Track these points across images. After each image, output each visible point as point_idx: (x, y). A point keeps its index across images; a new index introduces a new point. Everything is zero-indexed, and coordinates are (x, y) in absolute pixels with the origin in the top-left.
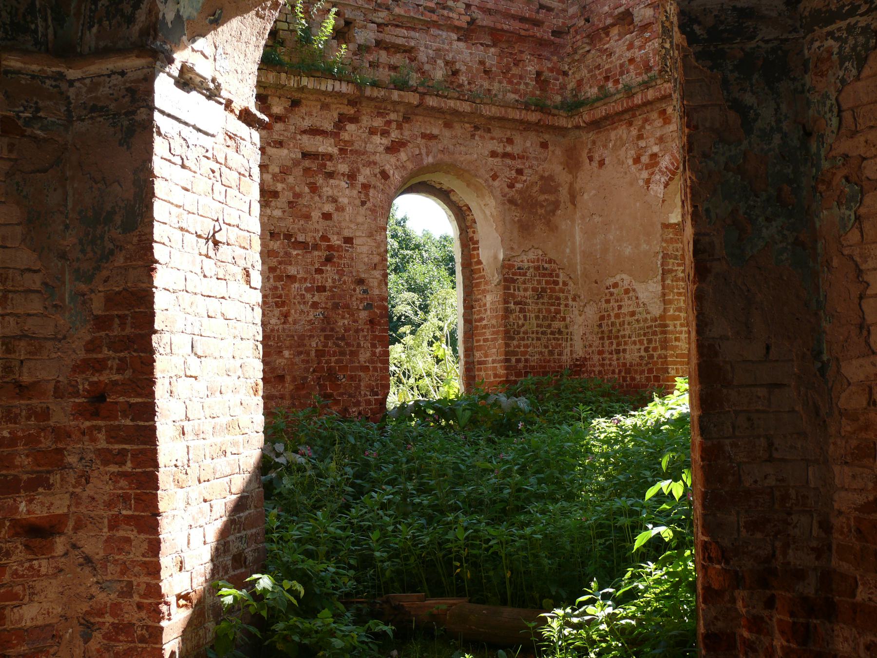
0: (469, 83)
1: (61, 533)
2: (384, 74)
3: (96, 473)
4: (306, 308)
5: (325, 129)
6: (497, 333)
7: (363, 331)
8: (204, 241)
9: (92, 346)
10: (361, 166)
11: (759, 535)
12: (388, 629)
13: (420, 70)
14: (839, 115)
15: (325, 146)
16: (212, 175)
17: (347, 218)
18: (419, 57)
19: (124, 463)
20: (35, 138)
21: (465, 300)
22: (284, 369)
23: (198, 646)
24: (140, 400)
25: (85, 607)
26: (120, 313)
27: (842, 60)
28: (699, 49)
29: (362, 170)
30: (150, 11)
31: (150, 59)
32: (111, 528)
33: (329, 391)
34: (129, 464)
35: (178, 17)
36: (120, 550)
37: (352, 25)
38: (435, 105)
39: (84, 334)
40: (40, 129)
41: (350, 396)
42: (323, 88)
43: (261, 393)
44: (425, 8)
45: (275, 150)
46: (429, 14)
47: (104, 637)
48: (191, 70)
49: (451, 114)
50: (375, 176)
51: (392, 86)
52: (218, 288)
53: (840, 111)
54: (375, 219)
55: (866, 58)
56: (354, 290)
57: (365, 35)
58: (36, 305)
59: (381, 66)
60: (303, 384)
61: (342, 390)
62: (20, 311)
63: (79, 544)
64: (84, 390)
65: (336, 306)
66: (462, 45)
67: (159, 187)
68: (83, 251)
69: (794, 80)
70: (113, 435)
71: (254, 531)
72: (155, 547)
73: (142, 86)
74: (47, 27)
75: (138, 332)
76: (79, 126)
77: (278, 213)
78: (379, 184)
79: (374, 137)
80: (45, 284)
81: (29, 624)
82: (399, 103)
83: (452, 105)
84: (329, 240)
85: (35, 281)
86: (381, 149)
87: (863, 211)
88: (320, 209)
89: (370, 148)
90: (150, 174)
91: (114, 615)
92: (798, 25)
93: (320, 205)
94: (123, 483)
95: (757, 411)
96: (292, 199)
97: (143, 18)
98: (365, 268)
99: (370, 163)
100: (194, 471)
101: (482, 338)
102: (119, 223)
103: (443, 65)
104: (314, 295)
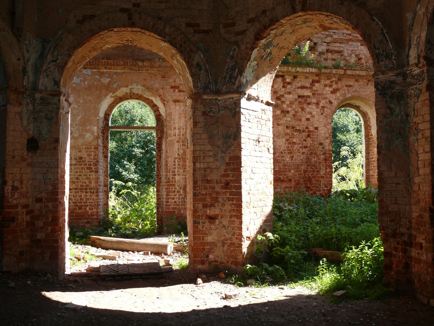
0: (366, 63)
1: (217, 219)
2: (330, 63)
3: (226, 204)
4: (300, 154)
5: (307, 86)
7: (322, 163)
8: (255, 141)
9: (226, 170)
10: (321, 99)
11: (392, 224)
12: (306, 253)
13: (345, 60)
14: (414, 111)
15: (307, 93)
16: (257, 122)
18: (344, 54)
19: (233, 201)
20: (211, 116)
21: (366, 150)
22: (291, 177)
23: (252, 251)
24: (238, 185)
25: (223, 238)
27: (415, 96)
28: (380, 92)
29: (321, 101)
30: (239, 82)
31: (239, 95)
32: (230, 218)
33: (308, 185)
34: (235, 201)
35: (247, 81)
36: (232, 224)
37: (317, 44)
38: (351, 73)
39: (224, 167)
40: (212, 113)
41: (317, 187)
42: (305, 71)
43: (273, 184)
44: (347, 34)
45: (288, 95)
46: (348, 36)
47: (228, 246)
48: (251, 95)
49: (358, 76)
50: (327, 103)
51: (333, 68)
52: (260, 154)
53: (414, 110)
54: (327, 120)
55: (419, 97)
56: (319, 147)
57: (322, 48)
58: (211, 160)
59: (329, 59)
60: (299, 183)
61: (313, 185)
62: (208, 161)
63: (222, 222)
64: (224, 182)
65: (311, 154)
67: (243, 129)
68: (223, 145)
69: (405, 100)
70: (231, 194)
71: (269, 224)
72: (241, 223)
73: (238, 102)
74: (213, 86)
75: (237, 167)
76: (222, 112)
77: (289, 119)
78: (328, 106)
80: (214, 154)
81: (209, 241)
82: (336, 74)
83: (358, 73)
84: (308, 128)
85: (211, 153)
87: (418, 137)
88: (305, 117)
89: (325, 92)
90: (240, 125)
91: (230, 240)
92: (406, 85)
93: (305, 115)
94: (233, 206)
95: (393, 190)
96: (294, 114)
97: (237, 83)
98: (323, 139)
99: (325, 98)
100: (252, 204)
101: (372, 166)
102: (232, 138)
103: (354, 56)
104: (303, 149)
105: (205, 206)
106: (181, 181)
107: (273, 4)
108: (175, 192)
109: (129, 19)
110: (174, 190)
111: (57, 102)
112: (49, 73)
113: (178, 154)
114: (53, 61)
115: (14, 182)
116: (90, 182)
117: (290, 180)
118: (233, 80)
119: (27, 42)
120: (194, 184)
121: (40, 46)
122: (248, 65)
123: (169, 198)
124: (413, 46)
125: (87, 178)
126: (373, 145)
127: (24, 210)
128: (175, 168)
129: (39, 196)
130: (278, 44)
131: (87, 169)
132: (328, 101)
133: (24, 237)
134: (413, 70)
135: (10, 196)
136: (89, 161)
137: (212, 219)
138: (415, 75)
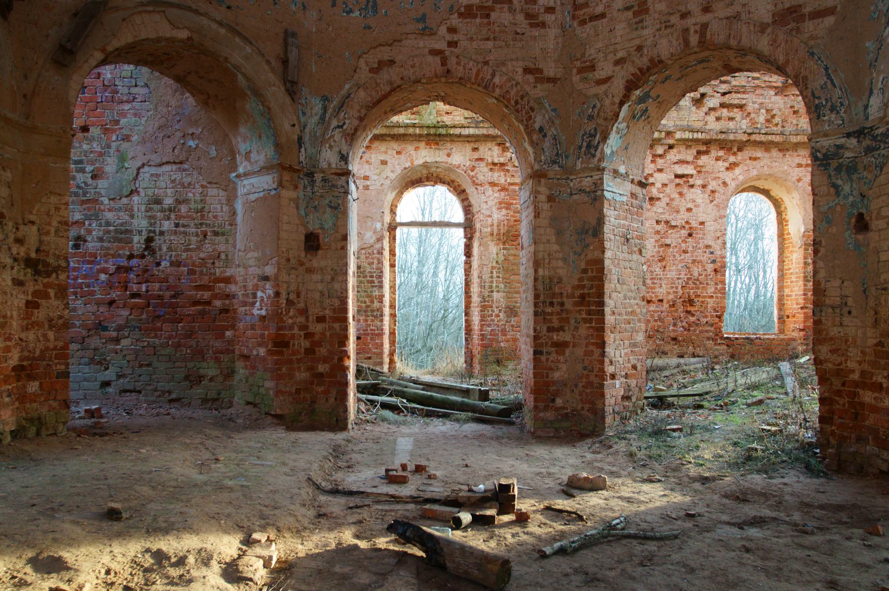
6: (799, 277)
9: (581, 279)
15: (689, 170)
17: (701, 210)
21: (779, 257)
26: (239, 218)
32: (586, 347)
66: (778, 98)
77: (660, 210)
79: (719, 162)
86: (723, 169)
94: (591, 330)
105: (550, 330)
106: (502, 300)
107: (655, 36)
108: (492, 316)
109: (442, 65)
110: (490, 313)
111: (344, 184)
112: (333, 144)
113: (497, 262)
114: (338, 127)
115: (289, 294)
116: (372, 302)
117: (661, 301)
118: (592, 151)
119: (303, 102)
120: (535, 299)
121: (320, 106)
122: (615, 128)
123: (484, 325)
124: (875, 91)
125: (368, 296)
126: (791, 249)
127: (302, 333)
128: (492, 282)
129: (322, 313)
130: (658, 96)
131: (368, 283)
132: (720, 182)
133: (302, 370)
134: (874, 128)
135: (284, 313)
136: (370, 272)
137: (561, 346)
138: (878, 135)
